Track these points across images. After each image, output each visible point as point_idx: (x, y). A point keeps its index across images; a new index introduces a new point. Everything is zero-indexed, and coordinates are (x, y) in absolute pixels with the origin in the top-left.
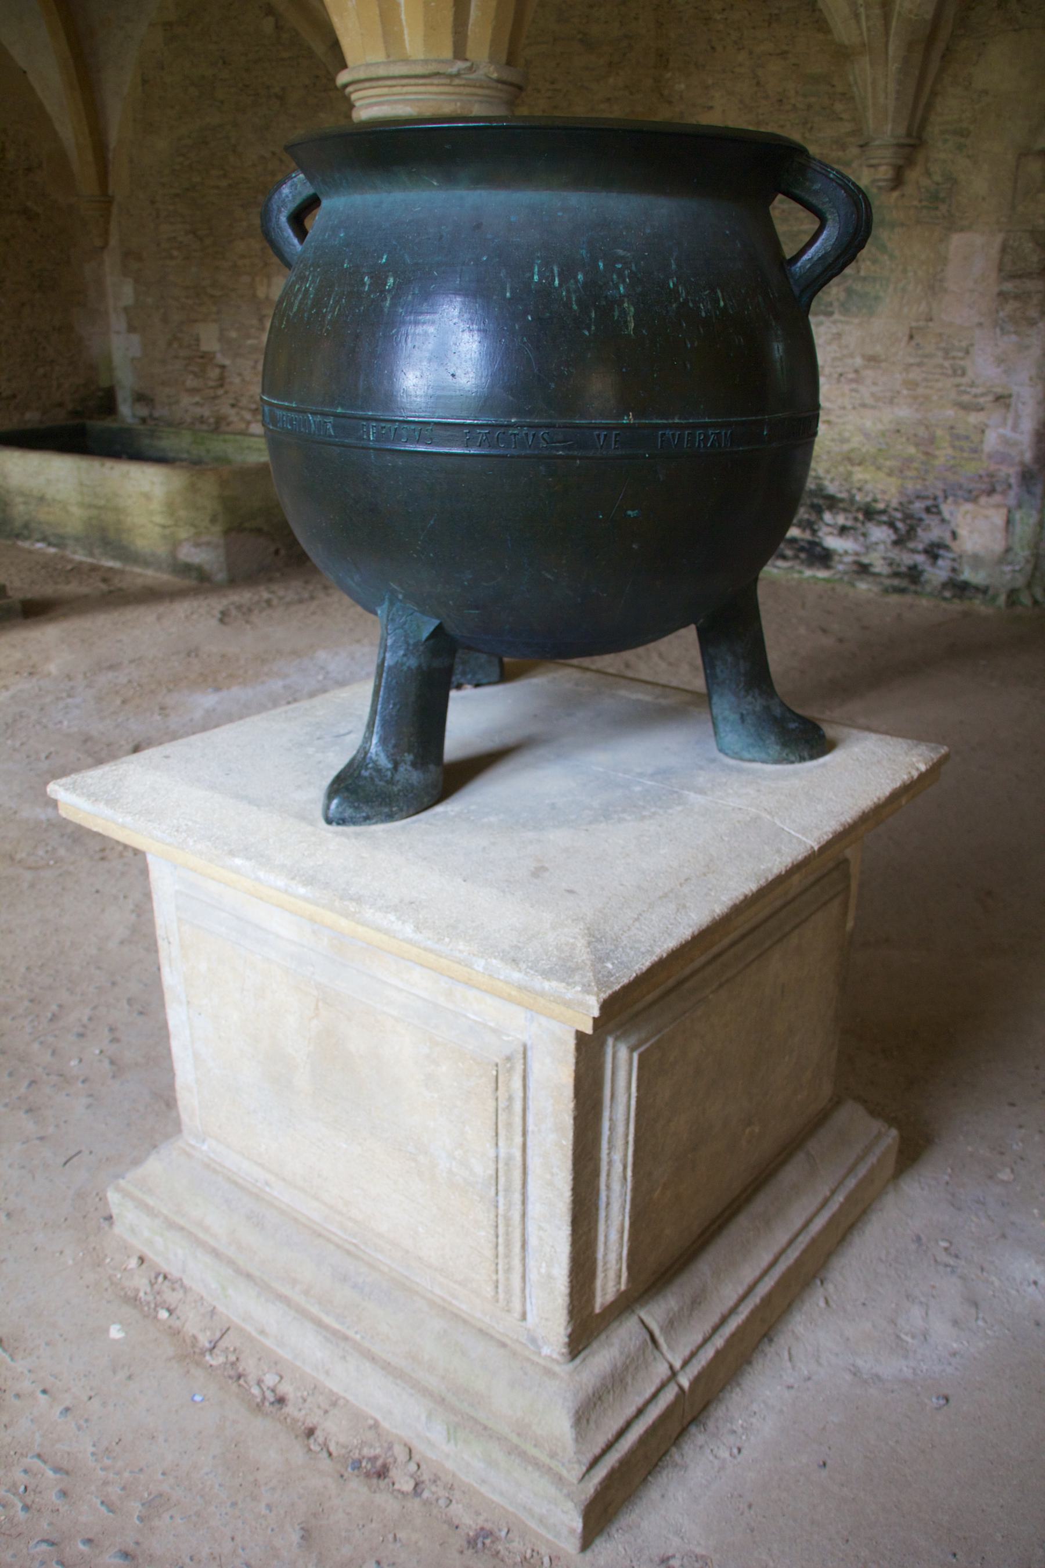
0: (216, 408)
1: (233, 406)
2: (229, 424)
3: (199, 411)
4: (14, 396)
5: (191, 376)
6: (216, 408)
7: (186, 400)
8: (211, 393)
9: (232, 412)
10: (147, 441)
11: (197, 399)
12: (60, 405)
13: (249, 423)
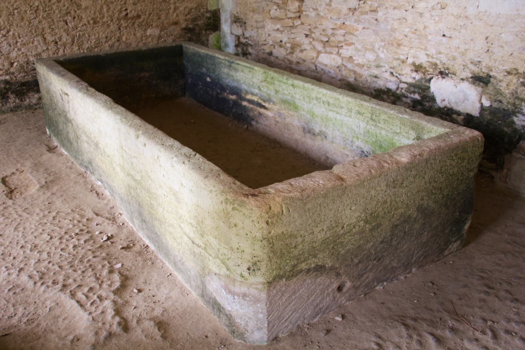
0: (293, 36)
1: (307, 36)
2: (302, 51)
3: (279, 36)
4: (139, 16)
5: (275, 7)
6: (293, 36)
7: (270, 26)
8: (290, 23)
9: (306, 41)
10: (226, 70)
11: (278, 26)
12: (176, 23)
13: (319, 53)
